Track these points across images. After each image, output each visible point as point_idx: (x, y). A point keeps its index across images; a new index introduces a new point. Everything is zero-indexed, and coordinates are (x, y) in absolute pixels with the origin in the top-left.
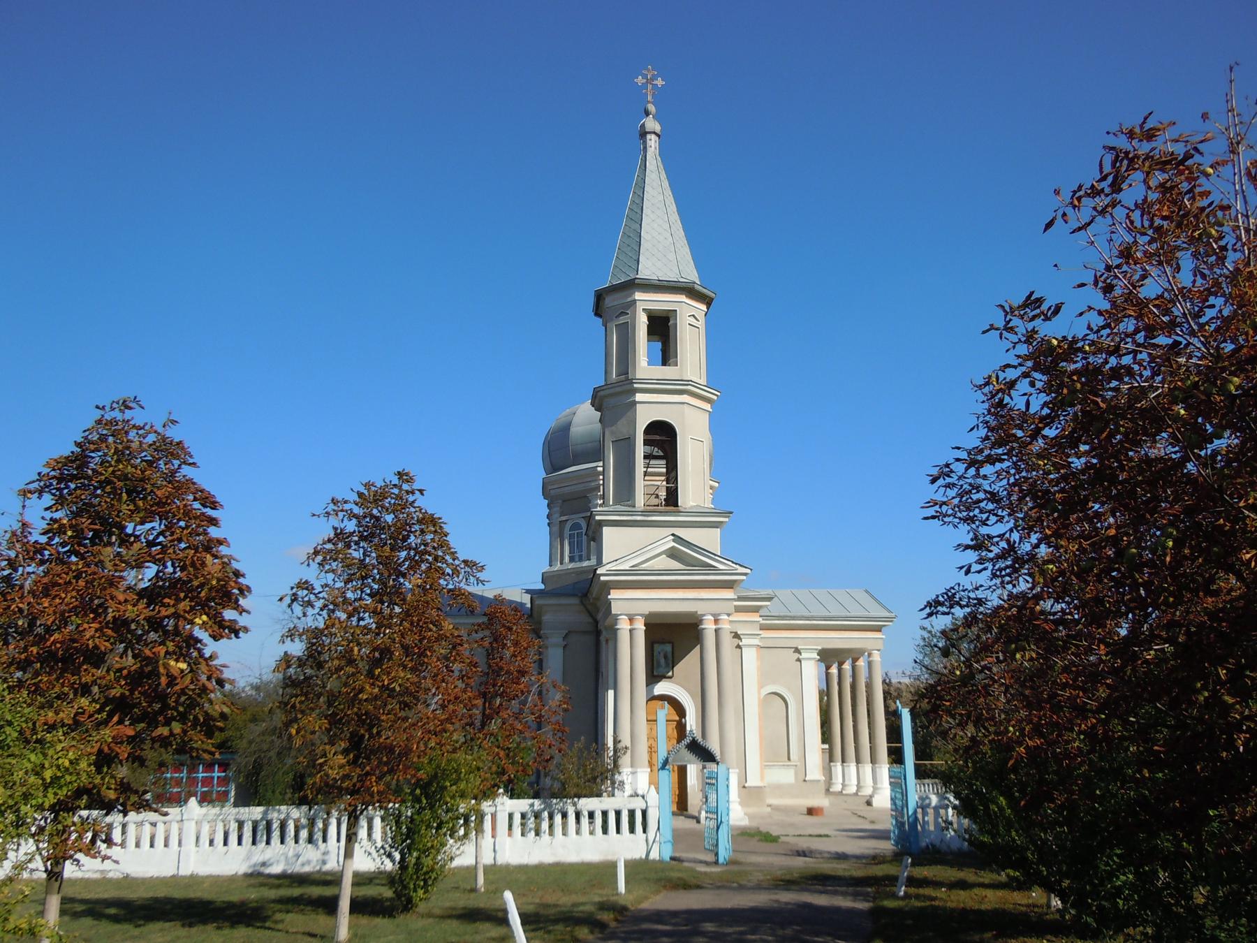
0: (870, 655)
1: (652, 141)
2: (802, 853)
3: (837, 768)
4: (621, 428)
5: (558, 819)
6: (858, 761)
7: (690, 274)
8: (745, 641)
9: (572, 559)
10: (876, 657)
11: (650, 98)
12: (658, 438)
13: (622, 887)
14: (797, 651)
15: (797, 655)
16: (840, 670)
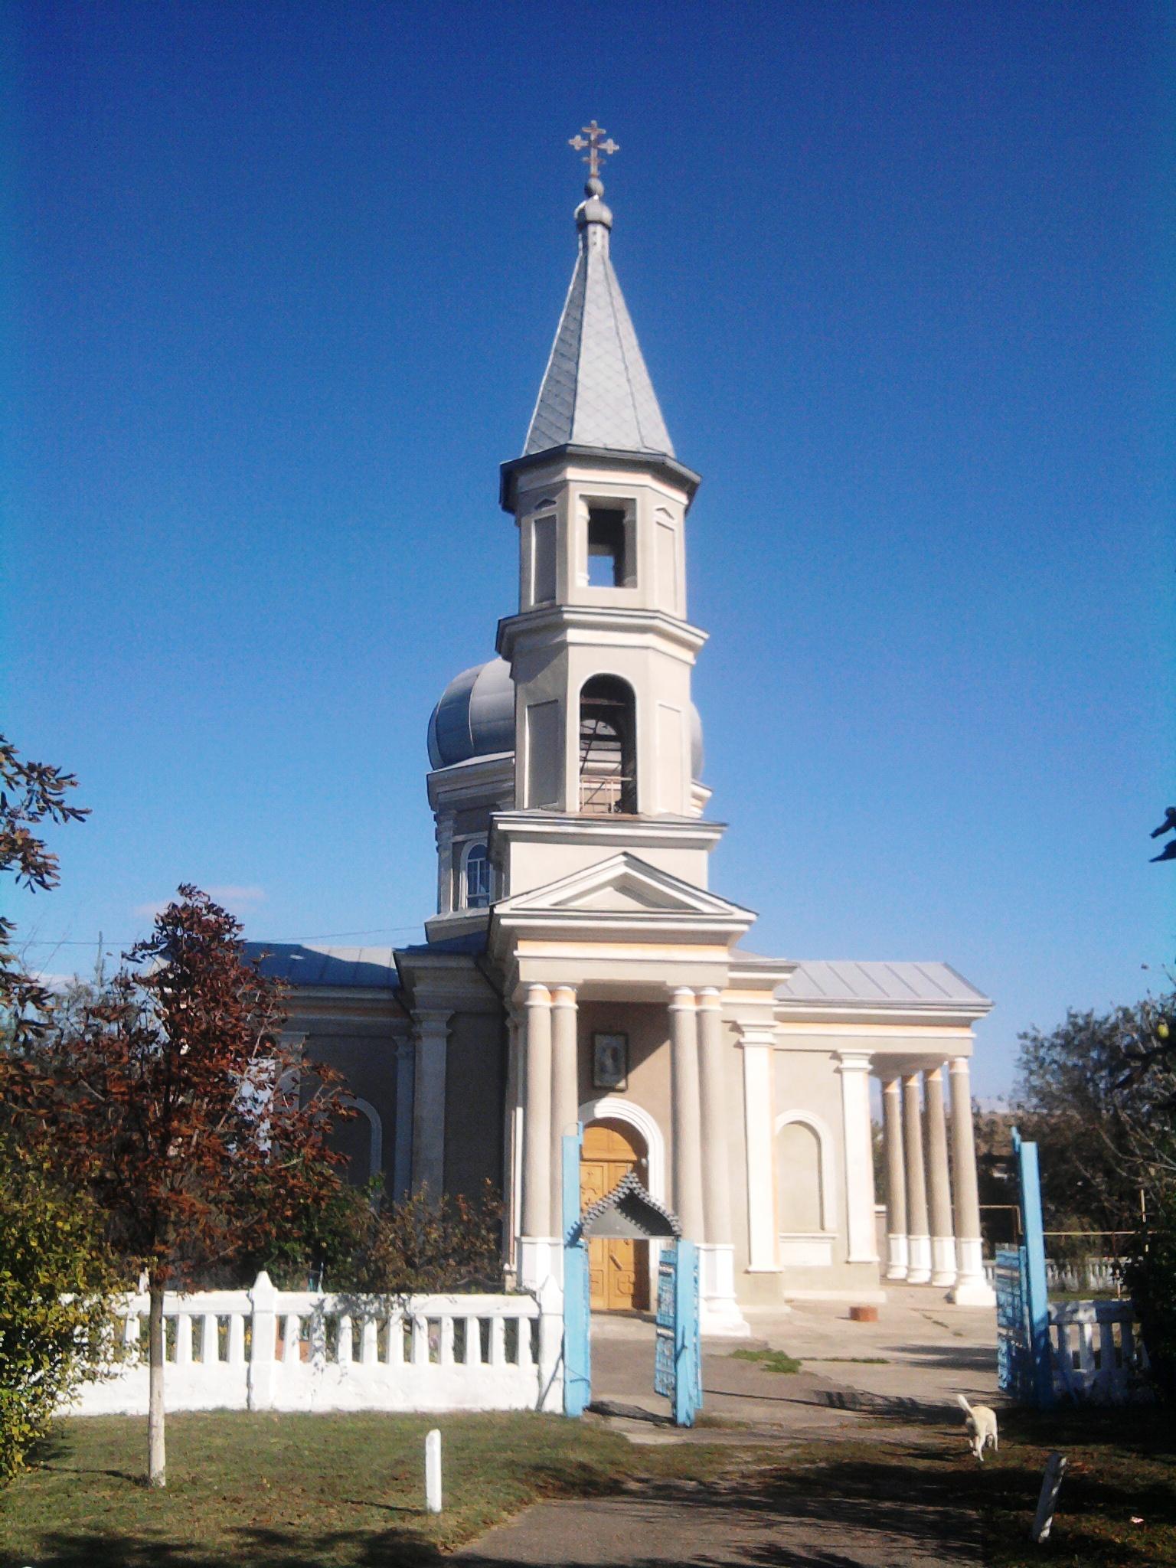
0: (952, 1064)
1: (599, 238)
2: (836, 1400)
3: (900, 1241)
4: (543, 681)
5: (371, 1330)
6: (933, 1231)
7: (659, 441)
8: (749, 1037)
9: (473, 903)
10: (962, 1068)
11: (594, 170)
12: (605, 702)
13: (435, 1497)
14: (836, 1056)
15: (835, 1063)
16: (904, 1090)
